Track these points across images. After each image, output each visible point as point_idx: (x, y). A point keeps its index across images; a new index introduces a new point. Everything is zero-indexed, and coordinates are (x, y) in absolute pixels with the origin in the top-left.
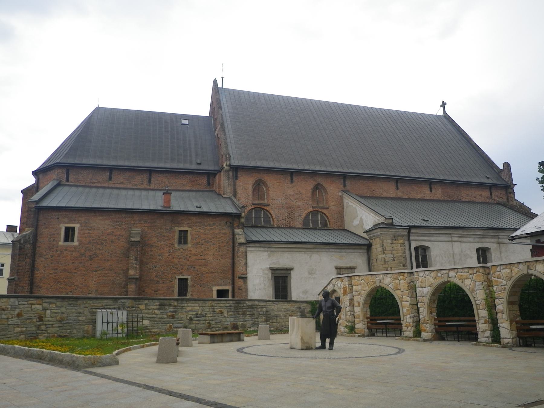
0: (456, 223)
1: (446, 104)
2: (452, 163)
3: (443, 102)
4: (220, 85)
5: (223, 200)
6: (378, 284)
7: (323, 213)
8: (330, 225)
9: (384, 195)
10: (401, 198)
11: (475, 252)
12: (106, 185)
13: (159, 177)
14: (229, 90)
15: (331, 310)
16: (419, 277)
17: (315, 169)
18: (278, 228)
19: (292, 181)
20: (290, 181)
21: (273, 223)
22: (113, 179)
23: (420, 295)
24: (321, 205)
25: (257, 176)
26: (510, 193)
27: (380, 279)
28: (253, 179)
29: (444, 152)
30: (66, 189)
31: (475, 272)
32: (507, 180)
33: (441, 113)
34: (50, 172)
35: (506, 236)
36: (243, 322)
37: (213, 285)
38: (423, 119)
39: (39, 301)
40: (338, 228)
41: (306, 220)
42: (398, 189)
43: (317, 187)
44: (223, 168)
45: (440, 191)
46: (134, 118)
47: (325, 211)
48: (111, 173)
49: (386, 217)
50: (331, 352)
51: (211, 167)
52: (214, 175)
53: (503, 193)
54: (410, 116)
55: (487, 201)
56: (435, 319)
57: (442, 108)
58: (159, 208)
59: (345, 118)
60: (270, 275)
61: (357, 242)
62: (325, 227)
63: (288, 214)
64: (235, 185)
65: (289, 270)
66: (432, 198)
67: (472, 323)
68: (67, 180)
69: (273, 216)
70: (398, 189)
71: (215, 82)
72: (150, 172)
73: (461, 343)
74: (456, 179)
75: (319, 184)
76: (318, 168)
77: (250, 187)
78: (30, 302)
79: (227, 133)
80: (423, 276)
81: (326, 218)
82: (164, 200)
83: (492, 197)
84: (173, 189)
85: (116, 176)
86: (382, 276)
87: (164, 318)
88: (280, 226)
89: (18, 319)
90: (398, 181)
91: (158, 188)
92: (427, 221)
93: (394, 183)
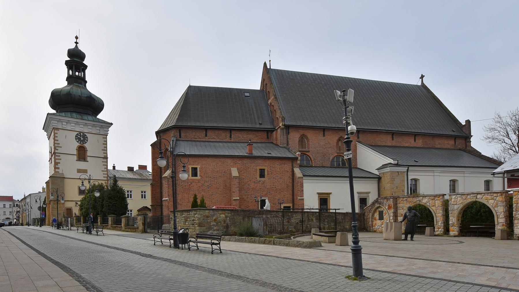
1: (424, 76)
2: (429, 120)
3: (422, 75)
4: (268, 67)
6: (418, 202)
9: (384, 144)
11: (484, 181)
15: (414, 218)
19: (324, 136)
20: (323, 135)
22: (208, 136)
23: (451, 210)
25: (302, 132)
26: (468, 142)
27: (420, 200)
28: (299, 134)
29: (423, 113)
31: (499, 195)
32: (467, 132)
33: (419, 84)
34: (168, 132)
35: (469, 172)
38: (412, 88)
39: (224, 212)
42: (393, 140)
48: (206, 132)
49: (394, 159)
51: (269, 126)
54: (398, 87)
55: (452, 148)
57: (421, 79)
63: (321, 158)
64: (287, 138)
65: (329, 194)
67: (493, 227)
68: (180, 137)
70: (393, 140)
71: (265, 64)
73: (479, 238)
75: (341, 137)
78: (219, 213)
80: (455, 198)
84: (245, 141)
85: (209, 133)
86: (421, 198)
88: (316, 165)
90: (393, 134)
91: (236, 141)
92: (418, 162)
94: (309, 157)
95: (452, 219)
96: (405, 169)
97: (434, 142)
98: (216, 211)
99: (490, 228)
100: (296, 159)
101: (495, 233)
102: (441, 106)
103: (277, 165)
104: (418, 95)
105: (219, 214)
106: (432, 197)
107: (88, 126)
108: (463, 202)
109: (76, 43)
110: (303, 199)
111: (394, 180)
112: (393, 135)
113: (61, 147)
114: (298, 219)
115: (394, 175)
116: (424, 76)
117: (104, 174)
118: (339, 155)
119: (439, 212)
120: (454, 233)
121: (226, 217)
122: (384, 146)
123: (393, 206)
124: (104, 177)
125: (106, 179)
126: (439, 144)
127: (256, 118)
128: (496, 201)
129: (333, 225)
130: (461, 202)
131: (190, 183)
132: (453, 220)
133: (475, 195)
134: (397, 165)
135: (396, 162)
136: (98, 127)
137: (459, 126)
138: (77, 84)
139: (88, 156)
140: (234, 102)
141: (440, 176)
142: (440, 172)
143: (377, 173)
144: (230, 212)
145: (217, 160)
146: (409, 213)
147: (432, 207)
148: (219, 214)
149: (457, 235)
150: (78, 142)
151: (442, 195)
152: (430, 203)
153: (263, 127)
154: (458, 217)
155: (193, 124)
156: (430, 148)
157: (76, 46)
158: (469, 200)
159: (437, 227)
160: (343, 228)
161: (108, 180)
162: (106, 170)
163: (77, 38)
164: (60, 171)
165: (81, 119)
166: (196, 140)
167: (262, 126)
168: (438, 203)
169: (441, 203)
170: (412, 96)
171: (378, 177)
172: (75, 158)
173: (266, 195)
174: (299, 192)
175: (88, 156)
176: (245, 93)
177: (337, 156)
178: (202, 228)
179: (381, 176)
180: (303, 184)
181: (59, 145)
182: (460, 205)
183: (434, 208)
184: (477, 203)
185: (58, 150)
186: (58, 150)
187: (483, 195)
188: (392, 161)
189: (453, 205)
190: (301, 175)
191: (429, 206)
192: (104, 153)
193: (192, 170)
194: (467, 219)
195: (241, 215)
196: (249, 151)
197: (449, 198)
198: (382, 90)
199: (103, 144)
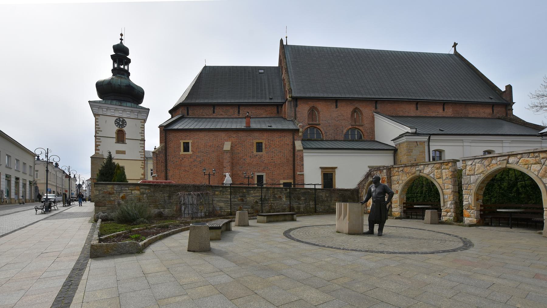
0: (467, 132)
1: (457, 44)
2: (461, 88)
3: (455, 43)
4: (285, 43)
5: (287, 122)
6: (418, 173)
7: (359, 129)
8: (364, 138)
9: (406, 114)
10: (419, 116)
12: (212, 117)
13: (245, 109)
14: (291, 46)
15: (382, 196)
16: (466, 165)
17: (354, 97)
18: (326, 141)
19: (337, 107)
20: (335, 107)
21: (323, 137)
23: (466, 183)
24: (357, 124)
25: (311, 104)
26: (509, 110)
27: (420, 169)
29: (455, 81)
30: (186, 120)
32: (508, 99)
33: (452, 52)
36: (298, 205)
37: (281, 179)
40: (370, 140)
41: (346, 134)
42: (417, 109)
43: (355, 110)
44: (287, 99)
45: (451, 110)
46: (228, 71)
47: (360, 128)
50: (380, 240)
51: (280, 101)
52: (282, 105)
53: (503, 109)
54: (427, 56)
55: (489, 117)
56: (481, 206)
58: (243, 127)
59: (376, 59)
60: (321, 173)
61: (386, 148)
62: (360, 139)
63: (333, 131)
65: (334, 168)
66: (444, 115)
68: (188, 114)
69: (323, 132)
70: (417, 109)
71: (282, 41)
72: (239, 106)
73: (513, 229)
74: (465, 100)
75: (356, 108)
76: (356, 96)
77: (306, 112)
79: (290, 75)
80: (471, 164)
81: (361, 133)
82: (246, 122)
83: (493, 114)
84: (254, 117)
85: (217, 110)
86: (422, 166)
87: (236, 201)
88: (328, 139)
89: (123, 201)
90: (417, 103)
92: (443, 130)
93: (414, 105)
94: (319, 131)
95: (467, 198)
96: (426, 138)
97: (466, 111)
98: (125, 187)
99: (534, 213)
100: (298, 130)
101: (543, 223)
102: (476, 73)
103: (276, 138)
104: (449, 63)
105: (130, 190)
106: (437, 164)
107: (126, 111)
108: (484, 171)
109: (121, 39)
110: (303, 175)
111: (412, 152)
112: (417, 104)
113: (101, 131)
114: (257, 196)
115: (411, 146)
116: (457, 44)
117: (141, 155)
118: (353, 128)
119: (448, 187)
120: (470, 221)
121: (143, 194)
122: (406, 116)
123: (386, 180)
124: (141, 158)
125: (143, 159)
126: (473, 112)
127: (267, 93)
128: (544, 166)
129: (312, 205)
130: (480, 171)
131: (181, 159)
132: (469, 199)
133: (504, 158)
134: (415, 134)
135: (414, 131)
136: (128, 111)
137: (498, 93)
138: (120, 76)
139: (126, 139)
140: (247, 79)
141: (471, 146)
142: (471, 141)
143: (393, 144)
144: (148, 187)
145: (211, 134)
146: (375, 188)
147: (438, 180)
148: (130, 190)
149: (475, 223)
150: (117, 126)
151: (452, 161)
152: (434, 174)
153: (273, 102)
154: (477, 194)
155: (202, 101)
156: (461, 118)
157: (121, 42)
158: (494, 166)
159: (445, 210)
160: (327, 208)
161: (144, 160)
162: (143, 151)
163: (122, 35)
164: (100, 152)
165: (120, 105)
166: (203, 117)
167: (272, 101)
168: (446, 173)
169: (450, 174)
170: (443, 65)
171: (394, 148)
172: (114, 140)
173: (263, 171)
174: (298, 166)
175: (126, 139)
176: (260, 70)
177: (352, 129)
178: (100, 208)
179: (397, 147)
180: (303, 157)
181: (99, 129)
182: (479, 175)
183: (440, 181)
184: (511, 172)
185: (98, 133)
186: (98, 133)
187: (519, 156)
188: (409, 130)
189: (468, 175)
190: (301, 148)
191: (434, 178)
192: (141, 136)
193: (184, 145)
194: (494, 198)
195: (166, 191)
196: (246, 123)
197: (462, 165)
198: (408, 60)
199: (141, 128)
